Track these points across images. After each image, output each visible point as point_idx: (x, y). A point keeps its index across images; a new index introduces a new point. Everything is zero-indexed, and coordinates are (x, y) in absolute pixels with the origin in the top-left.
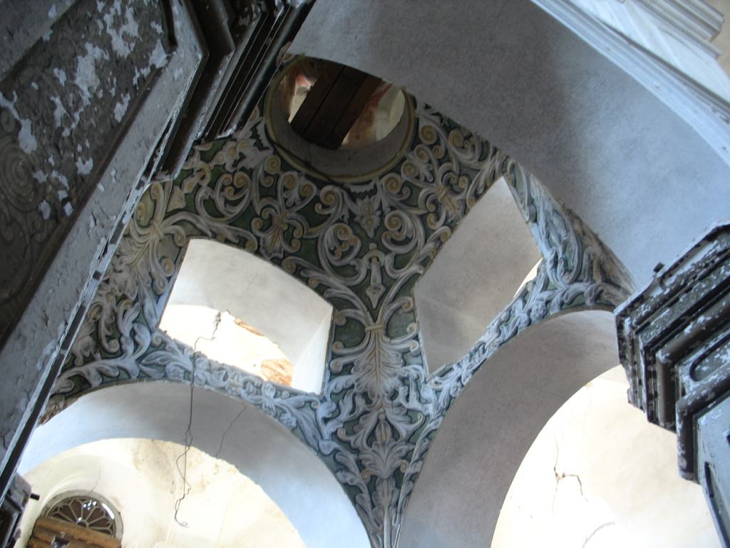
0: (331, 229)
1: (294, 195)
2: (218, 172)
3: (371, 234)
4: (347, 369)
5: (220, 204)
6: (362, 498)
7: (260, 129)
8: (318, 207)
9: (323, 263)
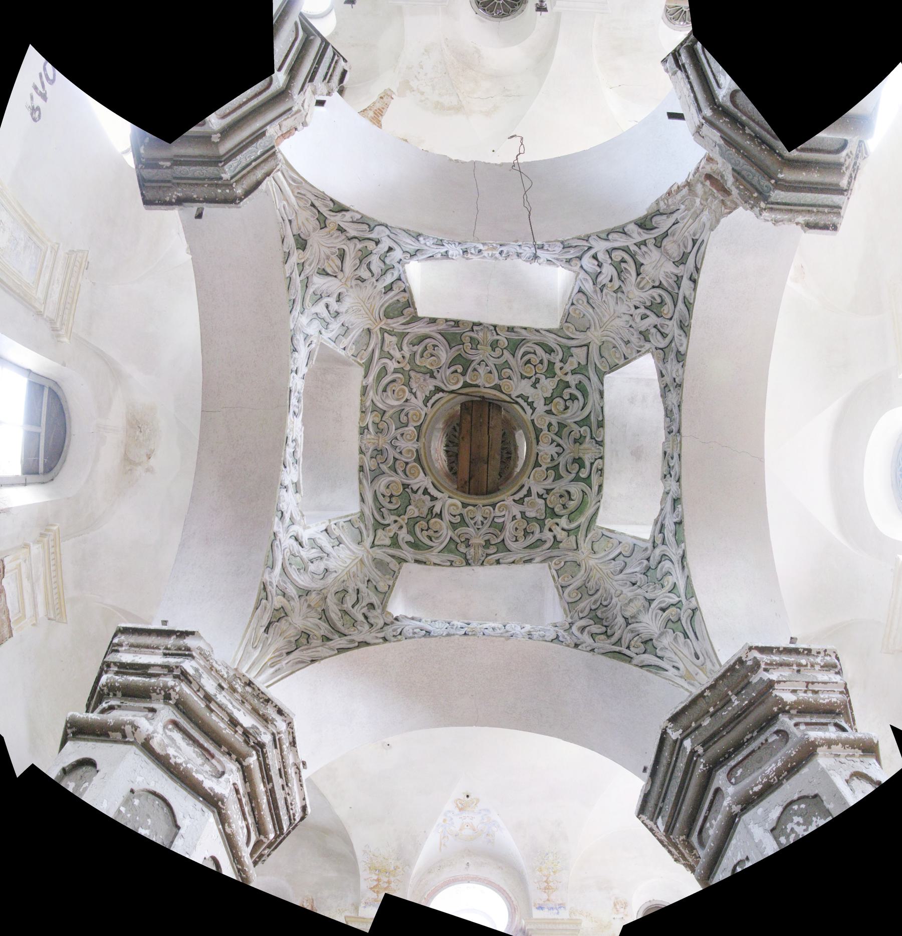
0: (443, 360)
1: (482, 370)
2: (550, 372)
3: (412, 374)
4: (389, 288)
5: (540, 351)
6: (326, 206)
7: (529, 411)
8: (460, 369)
9: (439, 337)
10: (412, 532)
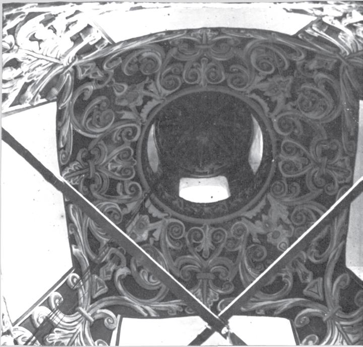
3: (291, 79)
7: (250, 215)
9: (336, 116)
10: (96, 93)
